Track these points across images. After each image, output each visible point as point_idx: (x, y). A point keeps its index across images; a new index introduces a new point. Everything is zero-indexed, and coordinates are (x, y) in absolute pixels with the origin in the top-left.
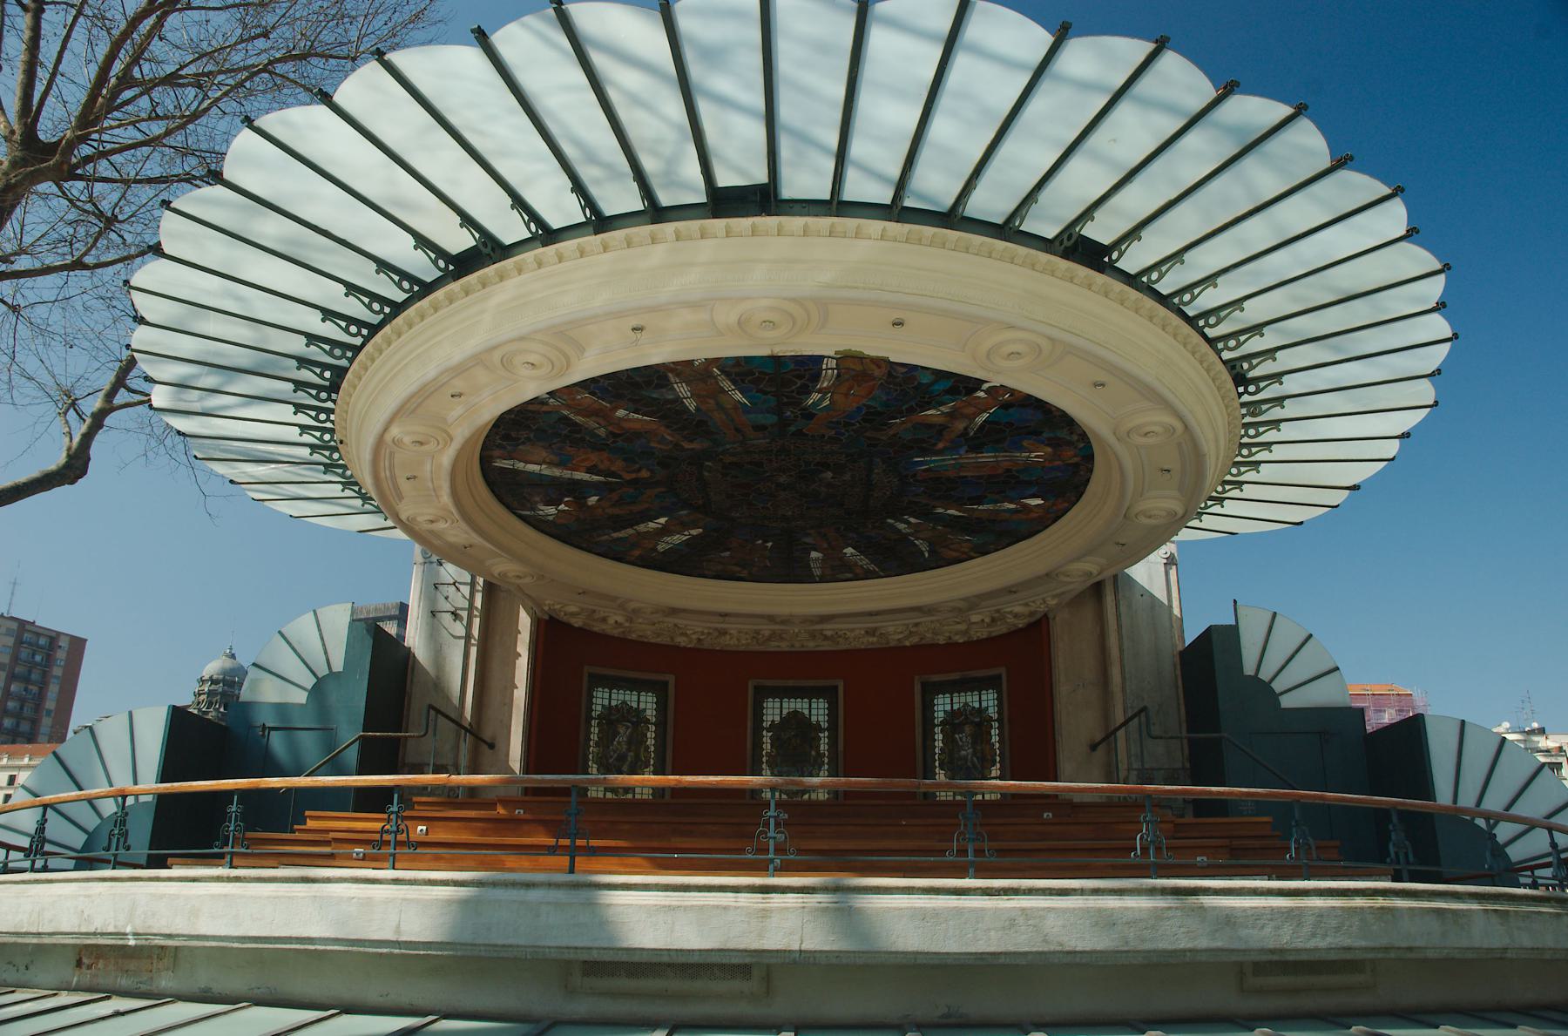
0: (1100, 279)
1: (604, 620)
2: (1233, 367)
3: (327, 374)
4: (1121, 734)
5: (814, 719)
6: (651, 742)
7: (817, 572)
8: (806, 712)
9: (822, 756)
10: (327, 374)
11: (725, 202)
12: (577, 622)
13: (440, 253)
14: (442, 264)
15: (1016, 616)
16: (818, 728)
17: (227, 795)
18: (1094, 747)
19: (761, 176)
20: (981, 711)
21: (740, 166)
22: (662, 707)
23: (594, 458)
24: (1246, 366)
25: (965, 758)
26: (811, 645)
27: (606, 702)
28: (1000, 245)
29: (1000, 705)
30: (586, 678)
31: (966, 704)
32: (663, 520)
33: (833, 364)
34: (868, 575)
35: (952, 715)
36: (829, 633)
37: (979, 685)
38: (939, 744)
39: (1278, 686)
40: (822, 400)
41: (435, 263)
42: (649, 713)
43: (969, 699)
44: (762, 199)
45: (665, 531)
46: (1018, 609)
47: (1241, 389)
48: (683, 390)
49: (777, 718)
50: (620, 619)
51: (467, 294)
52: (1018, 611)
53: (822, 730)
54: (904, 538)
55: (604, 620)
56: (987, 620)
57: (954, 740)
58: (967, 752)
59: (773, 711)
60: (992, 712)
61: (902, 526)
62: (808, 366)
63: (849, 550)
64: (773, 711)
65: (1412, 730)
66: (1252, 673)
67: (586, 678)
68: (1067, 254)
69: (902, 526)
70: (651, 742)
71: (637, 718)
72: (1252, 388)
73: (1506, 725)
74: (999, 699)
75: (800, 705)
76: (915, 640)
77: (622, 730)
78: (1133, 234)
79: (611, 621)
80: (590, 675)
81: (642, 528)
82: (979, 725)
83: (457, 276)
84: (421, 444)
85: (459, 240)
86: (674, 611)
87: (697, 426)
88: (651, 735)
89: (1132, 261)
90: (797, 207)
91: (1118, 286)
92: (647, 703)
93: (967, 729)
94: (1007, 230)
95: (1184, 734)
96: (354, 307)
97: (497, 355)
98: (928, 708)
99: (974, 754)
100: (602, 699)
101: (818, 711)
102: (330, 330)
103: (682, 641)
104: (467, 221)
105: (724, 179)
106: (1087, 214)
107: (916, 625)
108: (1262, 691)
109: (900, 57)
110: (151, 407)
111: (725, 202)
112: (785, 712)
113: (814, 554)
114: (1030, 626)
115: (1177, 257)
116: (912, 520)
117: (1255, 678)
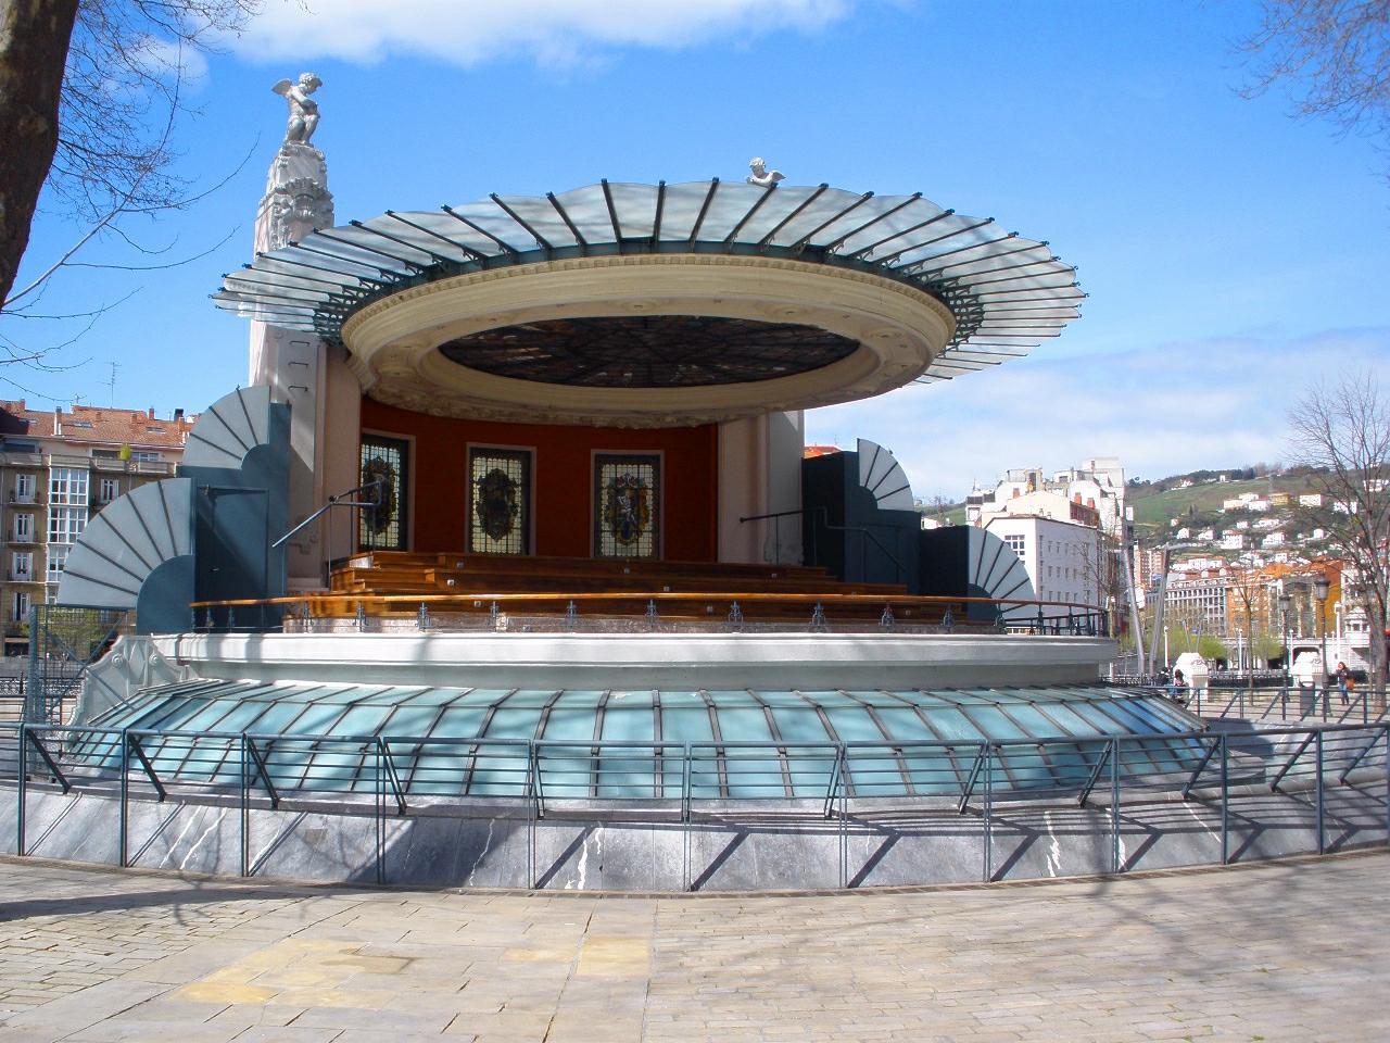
5: (510, 477)
6: (396, 490)
8: (505, 471)
9: (515, 506)
11: (625, 246)
16: (514, 484)
20: (388, 465)
21: (638, 216)
22: (526, 472)
25: (625, 515)
28: (757, 259)
30: (468, 451)
31: (379, 457)
33: (1316, 713)
35: (369, 462)
42: (647, 480)
43: (630, 471)
44: (652, 245)
53: (517, 486)
57: (617, 501)
64: (481, 468)
65: (331, 197)
66: (159, 563)
67: (468, 451)
70: (396, 490)
71: (384, 468)
80: (472, 449)
88: (649, 502)
93: (628, 493)
99: (632, 512)
100: (609, 473)
101: (513, 470)
105: (625, 234)
110: (1325, 599)
111: (625, 246)
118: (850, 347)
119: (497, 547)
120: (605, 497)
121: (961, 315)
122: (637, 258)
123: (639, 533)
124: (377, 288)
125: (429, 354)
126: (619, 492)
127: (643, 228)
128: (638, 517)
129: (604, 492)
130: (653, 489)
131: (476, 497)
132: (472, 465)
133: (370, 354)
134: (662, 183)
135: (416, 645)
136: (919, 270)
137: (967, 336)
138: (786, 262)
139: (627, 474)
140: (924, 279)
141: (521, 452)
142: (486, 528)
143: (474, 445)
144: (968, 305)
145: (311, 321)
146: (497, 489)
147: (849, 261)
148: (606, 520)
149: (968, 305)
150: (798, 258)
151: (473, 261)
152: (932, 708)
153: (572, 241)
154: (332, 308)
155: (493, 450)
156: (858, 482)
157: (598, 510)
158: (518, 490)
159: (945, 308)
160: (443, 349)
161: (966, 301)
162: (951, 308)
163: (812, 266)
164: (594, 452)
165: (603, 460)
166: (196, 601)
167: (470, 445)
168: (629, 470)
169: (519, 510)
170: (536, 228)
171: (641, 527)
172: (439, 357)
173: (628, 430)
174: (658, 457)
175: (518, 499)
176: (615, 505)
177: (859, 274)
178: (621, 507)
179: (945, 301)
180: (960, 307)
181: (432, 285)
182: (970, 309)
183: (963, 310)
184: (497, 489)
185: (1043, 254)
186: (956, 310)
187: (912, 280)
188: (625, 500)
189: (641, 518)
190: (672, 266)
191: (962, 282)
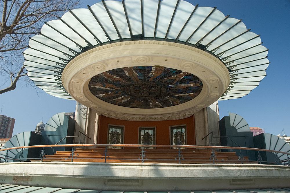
0: (204, 52)
1: (112, 115)
2: (229, 68)
3: (60, 70)
4: (208, 136)
5: (151, 134)
6: (120, 138)
7: (151, 107)
8: (149, 133)
9: (152, 141)
10: (60, 70)
11: (134, 38)
12: (106, 116)
13: (81, 47)
14: (81, 49)
15: (188, 115)
18: (203, 139)
19: (141, 33)
21: (137, 31)
23: (110, 85)
24: (231, 68)
26: (150, 120)
27: (112, 131)
29: (185, 131)
31: (179, 131)
32: (122, 97)
34: (161, 107)
36: (153, 118)
38: (174, 138)
39: (237, 128)
40: (152, 74)
41: (80, 49)
44: (141, 37)
45: (123, 99)
47: (230, 72)
48: (126, 73)
49: (144, 134)
50: (114, 115)
51: (86, 55)
52: (188, 114)
54: (167, 100)
55: (112, 115)
56: (183, 115)
57: (177, 138)
58: (179, 140)
59: (143, 132)
60: (184, 133)
61: (167, 98)
62: (150, 68)
64: (143, 132)
68: (198, 47)
69: (167, 98)
70: (120, 138)
71: (118, 134)
72: (232, 72)
75: (148, 131)
76: (169, 119)
77: (115, 136)
78: (210, 43)
79: (113, 116)
81: (119, 98)
82: (181, 135)
83: (84, 51)
84: (77, 82)
85: (85, 45)
86: (125, 114)
87: (129, 79)
89: (210, 48)
90: (147, 39)
91: (207, 53)
92: (120, 131)
93: (179, 135)
94: (186, 43)
95: (220, 137)
96: (65, 57)
97: (92, 66)
98: (172, 132)
100: (111, 130)
101: (151, 132)
102: (61, 61)
103: (126, 119)
104: (86, 41)
106: (201, 40)
107: (170, 116)
108: (234, 128)
109: (167, 11)
111: (134, 38)
112: (145, 132)
113: (151, 103)
115: (218, 48)
116: (169, 97)
120: (174, 137)
129: (174, 136)
130: (153, 136)
135: (83, 168)
139: (179, 131)
143: (124, 128)
146: (147, 137)
148: (174, 143)
164: (124, 126)
166: (73, 138)
169: (153, 141)
171: (183, 144)
173: (176, 120)
174: (155, 128)
175: (152, 139)
184: (147, 137)
188: (178, 137)
190: (190, 50)
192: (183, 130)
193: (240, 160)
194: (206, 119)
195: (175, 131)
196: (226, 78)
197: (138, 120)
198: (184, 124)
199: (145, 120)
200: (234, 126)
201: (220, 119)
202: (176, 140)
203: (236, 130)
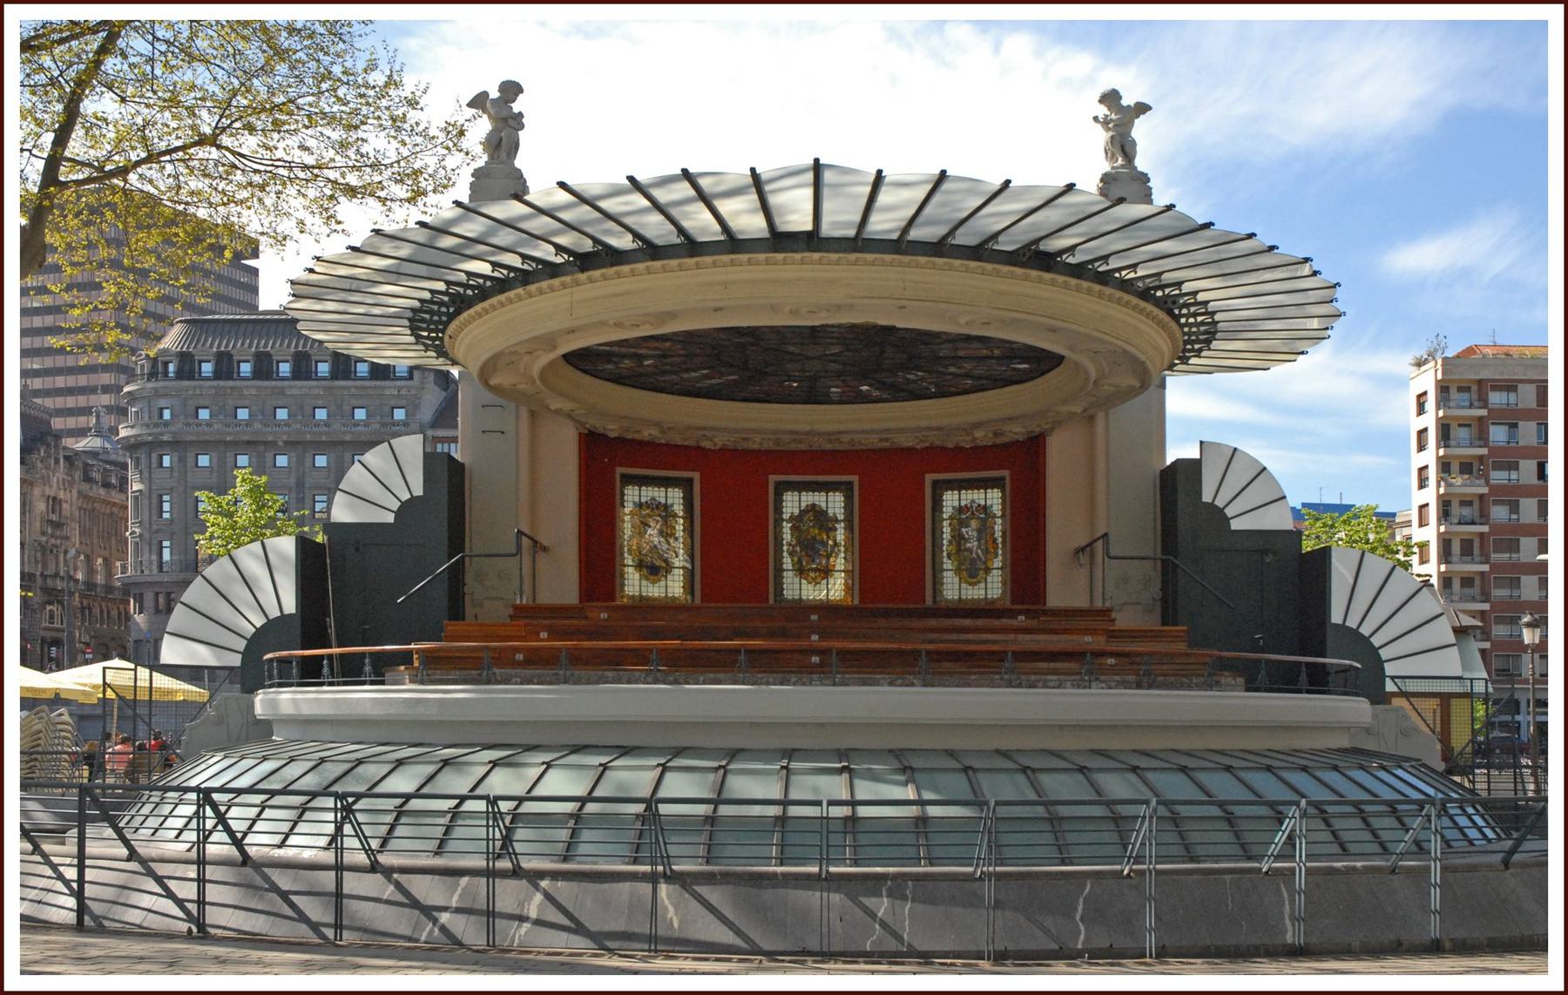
5: (831, 512)
8: (823, 505)
9: (836, 544)
12: (612, 435)
17: (363, 654)
19: (809, 227)
20: (985, 508)
29: (1004, 503)
35: (961, 510)
37: (985, 484)
38: (947, 536)
39: (1229, 512)
44: (811, 240)
45: (706, 377)
46: (1017, 429)
49: (796, 512)
52: (1017, 431)
59: (792, 503)
63: (865, 388)
71: (665, 511)
73: (1373, 80)
74: (1003, 498)
75: (818, 498)
80: (623, 476)
93: (974, 524)
95: (1159, 554)
98: (937, 505)
103: (707, 444)
105: (783, 227)
108: (1217, 516)
111: (779, 240)
112: (803, 505)
114: (1031, 439)
117: (1212, 505)
118: (1058, 360)
119: (974, 593)
120: (947, 530)
121: (1190, 325)
122: (798, 256)
123: (988, 570)
124: (489, 283)
125: (551, 364)
126: (963, 523)
127: (847, 225)
128: (986, 552)
131: (787, 535)
132: (623, 495)
133: (479, 364)
134: (880, 172)
136: (1132, 275)
137: (1200, 350)
138: (1005, 269)
139: (973, 501)
140: (1159, 293)
141: (841, 483)
142: (801, 571)
144: (1195, 315)
145: (406, 323)
147: (1079, 271)
148: (949, 557)
149: (1195, 315)
150: (1023, 265)
151: (568, 262)
152: (1101, 770)
153: (676, 239)
154: (436, 308)
155: (968, 481)
156: (1199, 493)
157: (937, 545)
158: (841, 527)
159: (1167, 318)
160: (581, 360)
161: (1192, 309)
162: (1182, 326)
163: (1034, 273)
164: (696, 476)
165: (940, 487)
167: (620, 470)
168: (975, 496)
170: (589, 230)
172: (563, 363)
176: (958, 538)
177: (1061, 279)
178: (966, 540)
179: (1176, 318)
180: (1188, 316)
181: (582, 277)
182: (1200, 319)
183: (1191, 320)
185: (1306, 270)
186: (1183, 320)
187: (1145, 295)
188: (970, 532)
189: (989, 552)
191: (1201, 297)
192: (994, 498)
193: (162, 403)
194: (1101, 487)
195: (951, 500)
196: (1161, 342)
197: (769, 445)
198: (1000, 467)
199: (803, 447)
200: (1220, 503)
201: (1168, 462)
202: (959, 544)
203: (1227, 520)
